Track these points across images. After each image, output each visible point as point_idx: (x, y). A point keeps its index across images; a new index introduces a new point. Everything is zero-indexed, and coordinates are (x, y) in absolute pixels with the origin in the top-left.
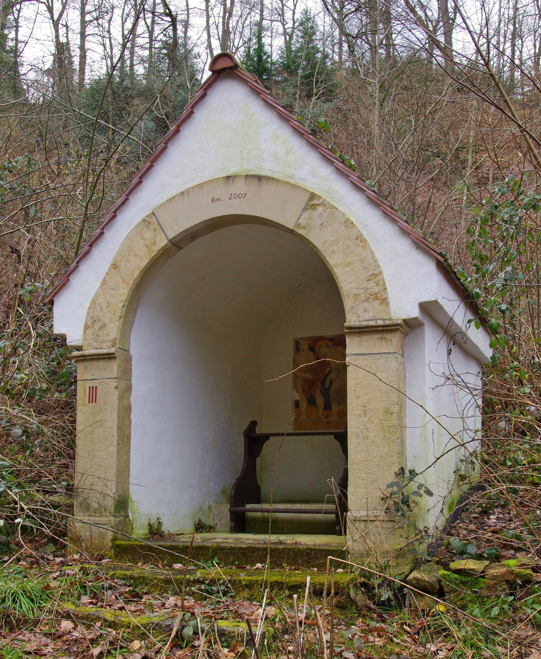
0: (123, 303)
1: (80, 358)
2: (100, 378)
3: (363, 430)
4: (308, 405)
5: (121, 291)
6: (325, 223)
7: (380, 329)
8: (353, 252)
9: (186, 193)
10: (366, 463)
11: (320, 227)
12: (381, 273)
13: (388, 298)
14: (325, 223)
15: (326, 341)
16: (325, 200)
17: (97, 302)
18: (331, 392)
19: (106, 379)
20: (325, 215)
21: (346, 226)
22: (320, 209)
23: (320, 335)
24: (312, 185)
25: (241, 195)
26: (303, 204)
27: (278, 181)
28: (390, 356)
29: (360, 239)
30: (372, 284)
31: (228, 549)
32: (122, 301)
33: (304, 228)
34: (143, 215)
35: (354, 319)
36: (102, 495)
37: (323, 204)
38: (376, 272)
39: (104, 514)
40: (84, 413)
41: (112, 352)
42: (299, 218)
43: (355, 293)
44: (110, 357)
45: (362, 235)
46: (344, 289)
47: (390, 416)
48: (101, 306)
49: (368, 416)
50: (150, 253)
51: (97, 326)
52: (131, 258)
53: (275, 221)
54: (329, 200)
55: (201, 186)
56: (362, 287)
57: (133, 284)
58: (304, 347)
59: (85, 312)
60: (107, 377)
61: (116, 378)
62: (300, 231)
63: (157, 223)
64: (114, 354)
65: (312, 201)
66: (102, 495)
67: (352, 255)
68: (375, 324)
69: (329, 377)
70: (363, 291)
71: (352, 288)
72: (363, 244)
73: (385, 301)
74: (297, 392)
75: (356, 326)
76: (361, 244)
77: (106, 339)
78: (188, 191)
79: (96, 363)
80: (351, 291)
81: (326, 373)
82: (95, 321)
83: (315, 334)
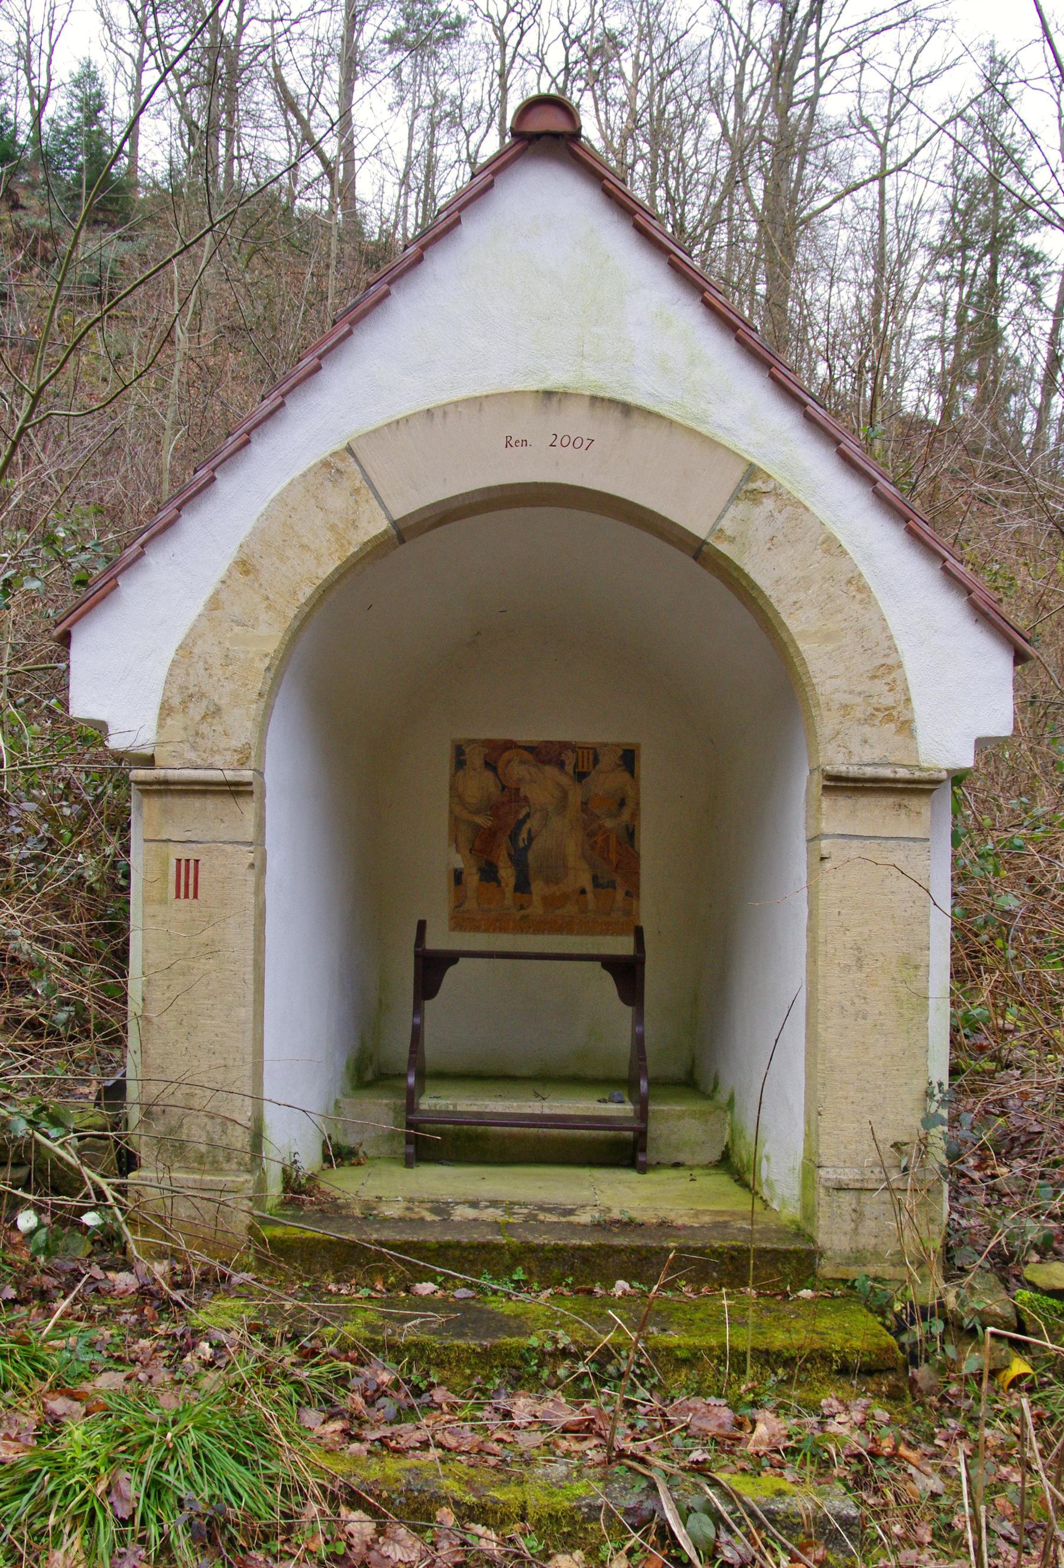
0: (267, 661)
1: (155, 787)
2: (208, 838)
3: (856, 1000)
4: (481, 880)
5: (263, 630)
6: (780, 537)
7: (900, 786)
8: (840, 611)
9: (439, 414)
10: (860, 1069)
11: (769, 545)
12: (900, 666)
13: (912, 721)
14: (780, 537)
15: (521, 751)
16: (781, 486)
17: (196, 651)
18: (530, 856)
19: (224, 842)
20: (780, 518)
21: (827, 551)
22: (769, 503)
23: (508, 737)
24: (749, 445)
25: (565, 442)
26: (729, 488)
27: (671, 423)
28: (917, 845)
29: (856, 583)
30: (880, 686)
31: (550, 1251)
32: (266, 656)
33: (732, 540)
34: (324, 451)
35: (840, 758)
36: (219, 1120)
37: (776, 493)
38: (890, 661)
39: (225, 1166)
40: (164, 923)
41: (246, 780)
42: (720, 517)
43: (844, 702)
44: (236, 790)
45: (860, 575)
46: (819, 689)
47: (912, 972)
48: (206, 662)
49: (867, 970)
50: (342, 546)
51: (196, 711)
52: (289, 553)
53: (663, 513)
54: (788, 486)
55: (478, 402)
56: (859, 689)
57: (296, 616)
58: (475, 759)
59: (163, 672)
60: (226, 838)
61: (251, 844)
62: (723, 547)
63: (360, 476)
64: (250, 784)
65: (751, 483)
66: (219, 1120)
67: (840, 616)
68: (892, 775)
69: (527, 826)
70: (859, 700)
71: (837, 690)
72: (864, 596)
73: (906, 727)
74: (458, 851)
75: (851, 775)
76: (859, 596)
77: (222, 746)
78: (444, 410)
79: (197, 802)
80: (836, 696)
81: (521, 817)
82: (191, 696)
83: (499, 734)
